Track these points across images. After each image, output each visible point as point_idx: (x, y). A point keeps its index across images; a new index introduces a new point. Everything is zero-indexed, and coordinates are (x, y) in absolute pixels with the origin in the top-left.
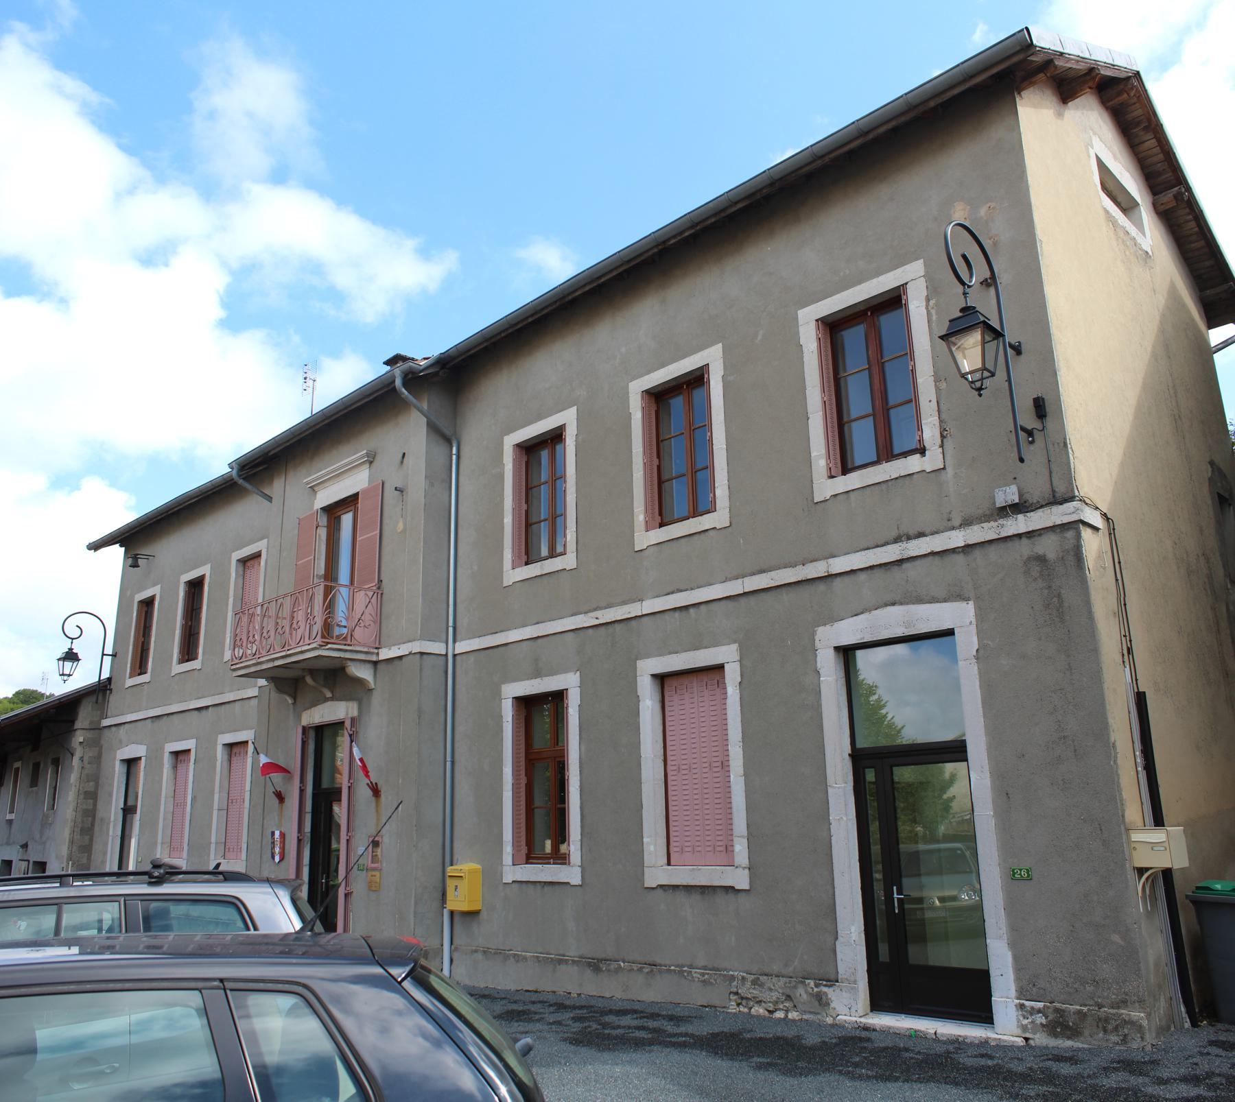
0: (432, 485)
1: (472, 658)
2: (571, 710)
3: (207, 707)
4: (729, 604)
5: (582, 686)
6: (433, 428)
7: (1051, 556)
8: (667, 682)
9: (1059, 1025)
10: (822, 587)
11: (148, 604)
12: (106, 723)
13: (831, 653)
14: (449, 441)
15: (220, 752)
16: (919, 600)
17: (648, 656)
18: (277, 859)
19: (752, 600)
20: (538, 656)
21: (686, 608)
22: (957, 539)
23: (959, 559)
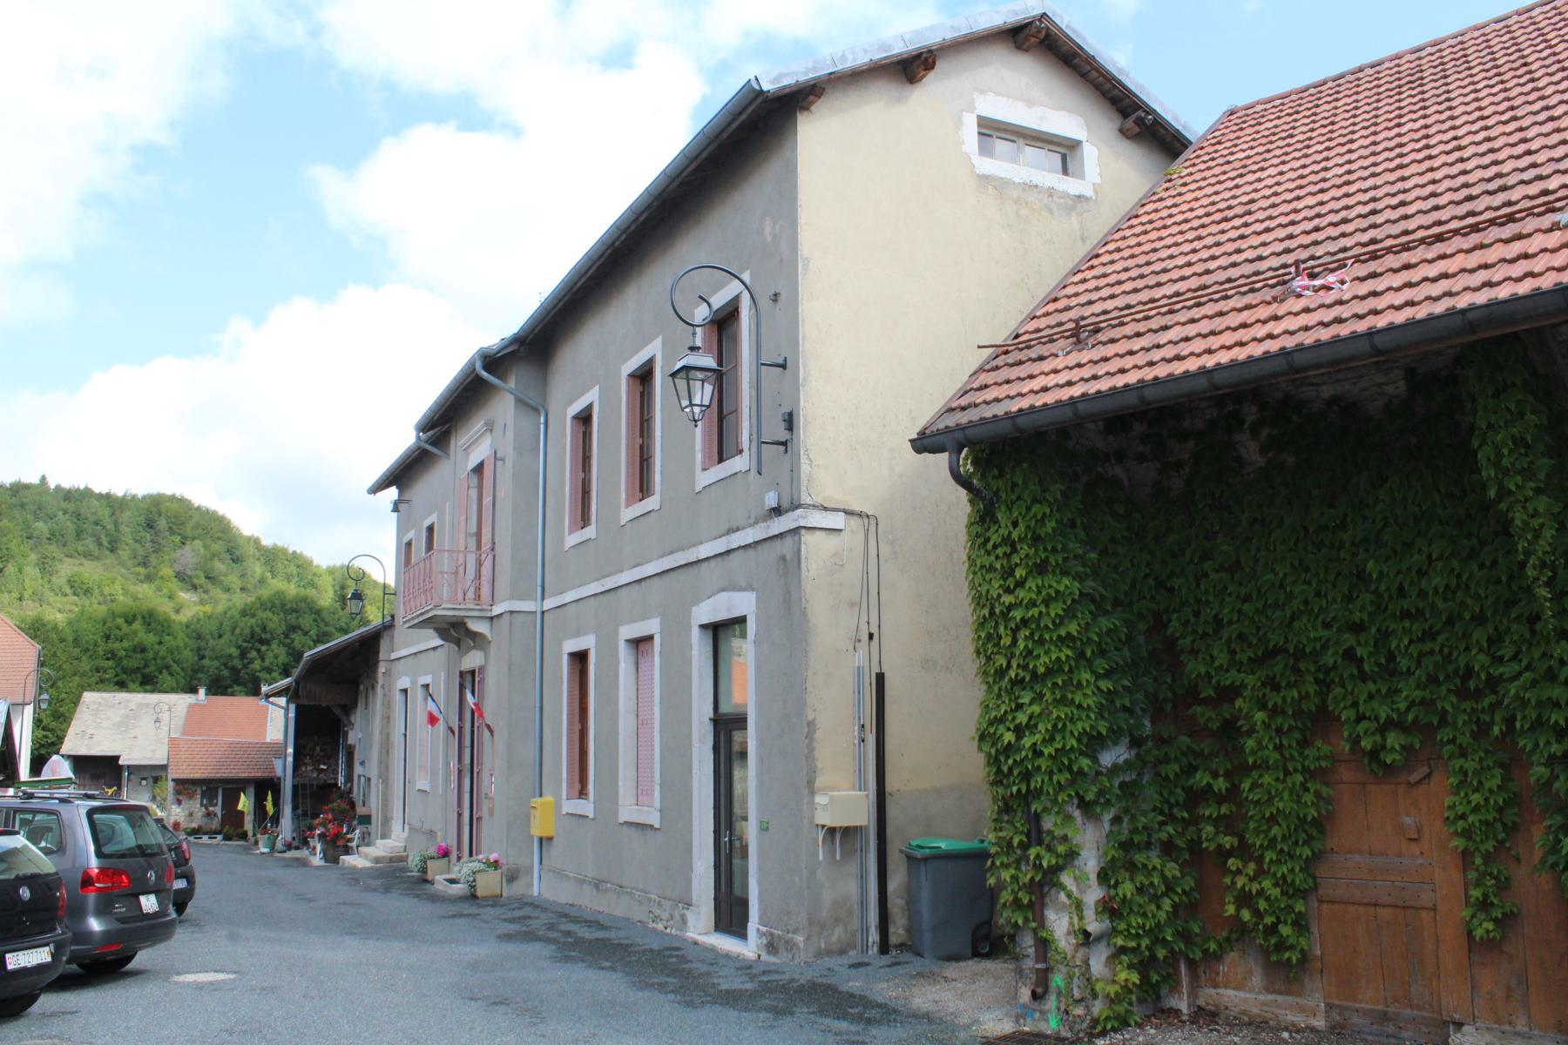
0: (521, 454)
6: (520, 401)
9: (771, 947)
11: (409, 544)
12: (393, 656)
14: (537, 411)
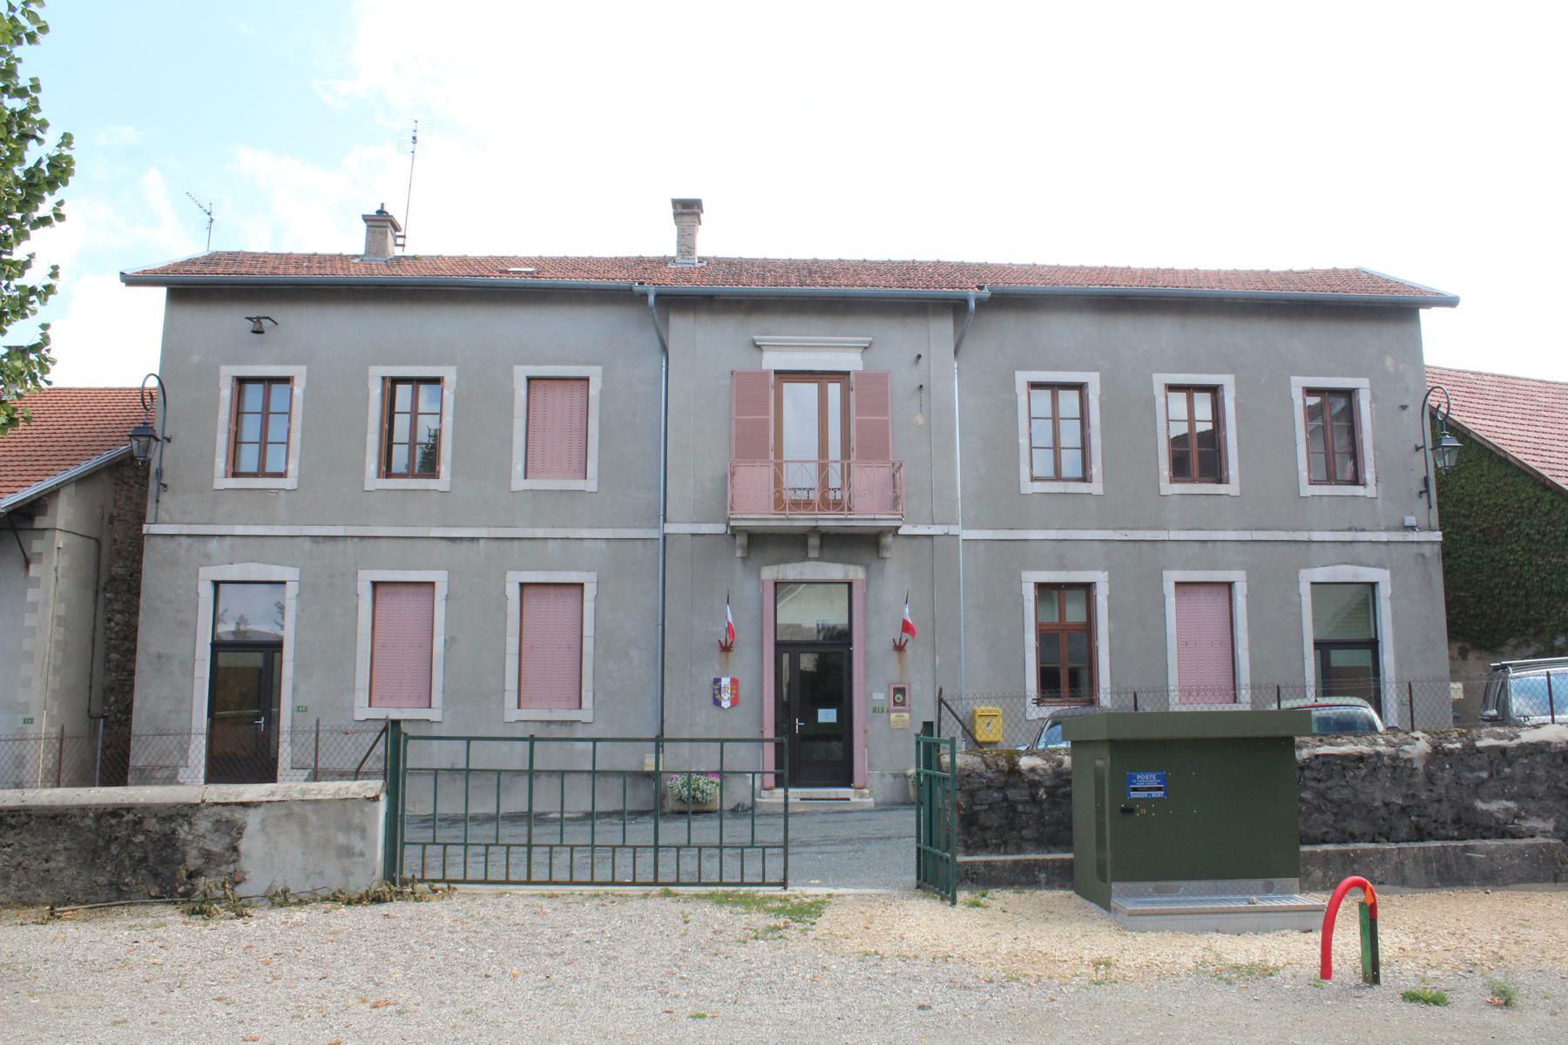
1: (982, 546)
2: (1099, 598)
3: (461, 539)
4: (1240, 546)
5: (1111, 581)
7: (1428, 554)
8: (380, 590)
10: (1303, 546)
13: (1032, 586)
15: (513, 592)
16: (1361, 564)
17: (1171, 568)
18: (725, 681)
19: (1256, 546)
20: (1061, 553)
22: (1383, 536)
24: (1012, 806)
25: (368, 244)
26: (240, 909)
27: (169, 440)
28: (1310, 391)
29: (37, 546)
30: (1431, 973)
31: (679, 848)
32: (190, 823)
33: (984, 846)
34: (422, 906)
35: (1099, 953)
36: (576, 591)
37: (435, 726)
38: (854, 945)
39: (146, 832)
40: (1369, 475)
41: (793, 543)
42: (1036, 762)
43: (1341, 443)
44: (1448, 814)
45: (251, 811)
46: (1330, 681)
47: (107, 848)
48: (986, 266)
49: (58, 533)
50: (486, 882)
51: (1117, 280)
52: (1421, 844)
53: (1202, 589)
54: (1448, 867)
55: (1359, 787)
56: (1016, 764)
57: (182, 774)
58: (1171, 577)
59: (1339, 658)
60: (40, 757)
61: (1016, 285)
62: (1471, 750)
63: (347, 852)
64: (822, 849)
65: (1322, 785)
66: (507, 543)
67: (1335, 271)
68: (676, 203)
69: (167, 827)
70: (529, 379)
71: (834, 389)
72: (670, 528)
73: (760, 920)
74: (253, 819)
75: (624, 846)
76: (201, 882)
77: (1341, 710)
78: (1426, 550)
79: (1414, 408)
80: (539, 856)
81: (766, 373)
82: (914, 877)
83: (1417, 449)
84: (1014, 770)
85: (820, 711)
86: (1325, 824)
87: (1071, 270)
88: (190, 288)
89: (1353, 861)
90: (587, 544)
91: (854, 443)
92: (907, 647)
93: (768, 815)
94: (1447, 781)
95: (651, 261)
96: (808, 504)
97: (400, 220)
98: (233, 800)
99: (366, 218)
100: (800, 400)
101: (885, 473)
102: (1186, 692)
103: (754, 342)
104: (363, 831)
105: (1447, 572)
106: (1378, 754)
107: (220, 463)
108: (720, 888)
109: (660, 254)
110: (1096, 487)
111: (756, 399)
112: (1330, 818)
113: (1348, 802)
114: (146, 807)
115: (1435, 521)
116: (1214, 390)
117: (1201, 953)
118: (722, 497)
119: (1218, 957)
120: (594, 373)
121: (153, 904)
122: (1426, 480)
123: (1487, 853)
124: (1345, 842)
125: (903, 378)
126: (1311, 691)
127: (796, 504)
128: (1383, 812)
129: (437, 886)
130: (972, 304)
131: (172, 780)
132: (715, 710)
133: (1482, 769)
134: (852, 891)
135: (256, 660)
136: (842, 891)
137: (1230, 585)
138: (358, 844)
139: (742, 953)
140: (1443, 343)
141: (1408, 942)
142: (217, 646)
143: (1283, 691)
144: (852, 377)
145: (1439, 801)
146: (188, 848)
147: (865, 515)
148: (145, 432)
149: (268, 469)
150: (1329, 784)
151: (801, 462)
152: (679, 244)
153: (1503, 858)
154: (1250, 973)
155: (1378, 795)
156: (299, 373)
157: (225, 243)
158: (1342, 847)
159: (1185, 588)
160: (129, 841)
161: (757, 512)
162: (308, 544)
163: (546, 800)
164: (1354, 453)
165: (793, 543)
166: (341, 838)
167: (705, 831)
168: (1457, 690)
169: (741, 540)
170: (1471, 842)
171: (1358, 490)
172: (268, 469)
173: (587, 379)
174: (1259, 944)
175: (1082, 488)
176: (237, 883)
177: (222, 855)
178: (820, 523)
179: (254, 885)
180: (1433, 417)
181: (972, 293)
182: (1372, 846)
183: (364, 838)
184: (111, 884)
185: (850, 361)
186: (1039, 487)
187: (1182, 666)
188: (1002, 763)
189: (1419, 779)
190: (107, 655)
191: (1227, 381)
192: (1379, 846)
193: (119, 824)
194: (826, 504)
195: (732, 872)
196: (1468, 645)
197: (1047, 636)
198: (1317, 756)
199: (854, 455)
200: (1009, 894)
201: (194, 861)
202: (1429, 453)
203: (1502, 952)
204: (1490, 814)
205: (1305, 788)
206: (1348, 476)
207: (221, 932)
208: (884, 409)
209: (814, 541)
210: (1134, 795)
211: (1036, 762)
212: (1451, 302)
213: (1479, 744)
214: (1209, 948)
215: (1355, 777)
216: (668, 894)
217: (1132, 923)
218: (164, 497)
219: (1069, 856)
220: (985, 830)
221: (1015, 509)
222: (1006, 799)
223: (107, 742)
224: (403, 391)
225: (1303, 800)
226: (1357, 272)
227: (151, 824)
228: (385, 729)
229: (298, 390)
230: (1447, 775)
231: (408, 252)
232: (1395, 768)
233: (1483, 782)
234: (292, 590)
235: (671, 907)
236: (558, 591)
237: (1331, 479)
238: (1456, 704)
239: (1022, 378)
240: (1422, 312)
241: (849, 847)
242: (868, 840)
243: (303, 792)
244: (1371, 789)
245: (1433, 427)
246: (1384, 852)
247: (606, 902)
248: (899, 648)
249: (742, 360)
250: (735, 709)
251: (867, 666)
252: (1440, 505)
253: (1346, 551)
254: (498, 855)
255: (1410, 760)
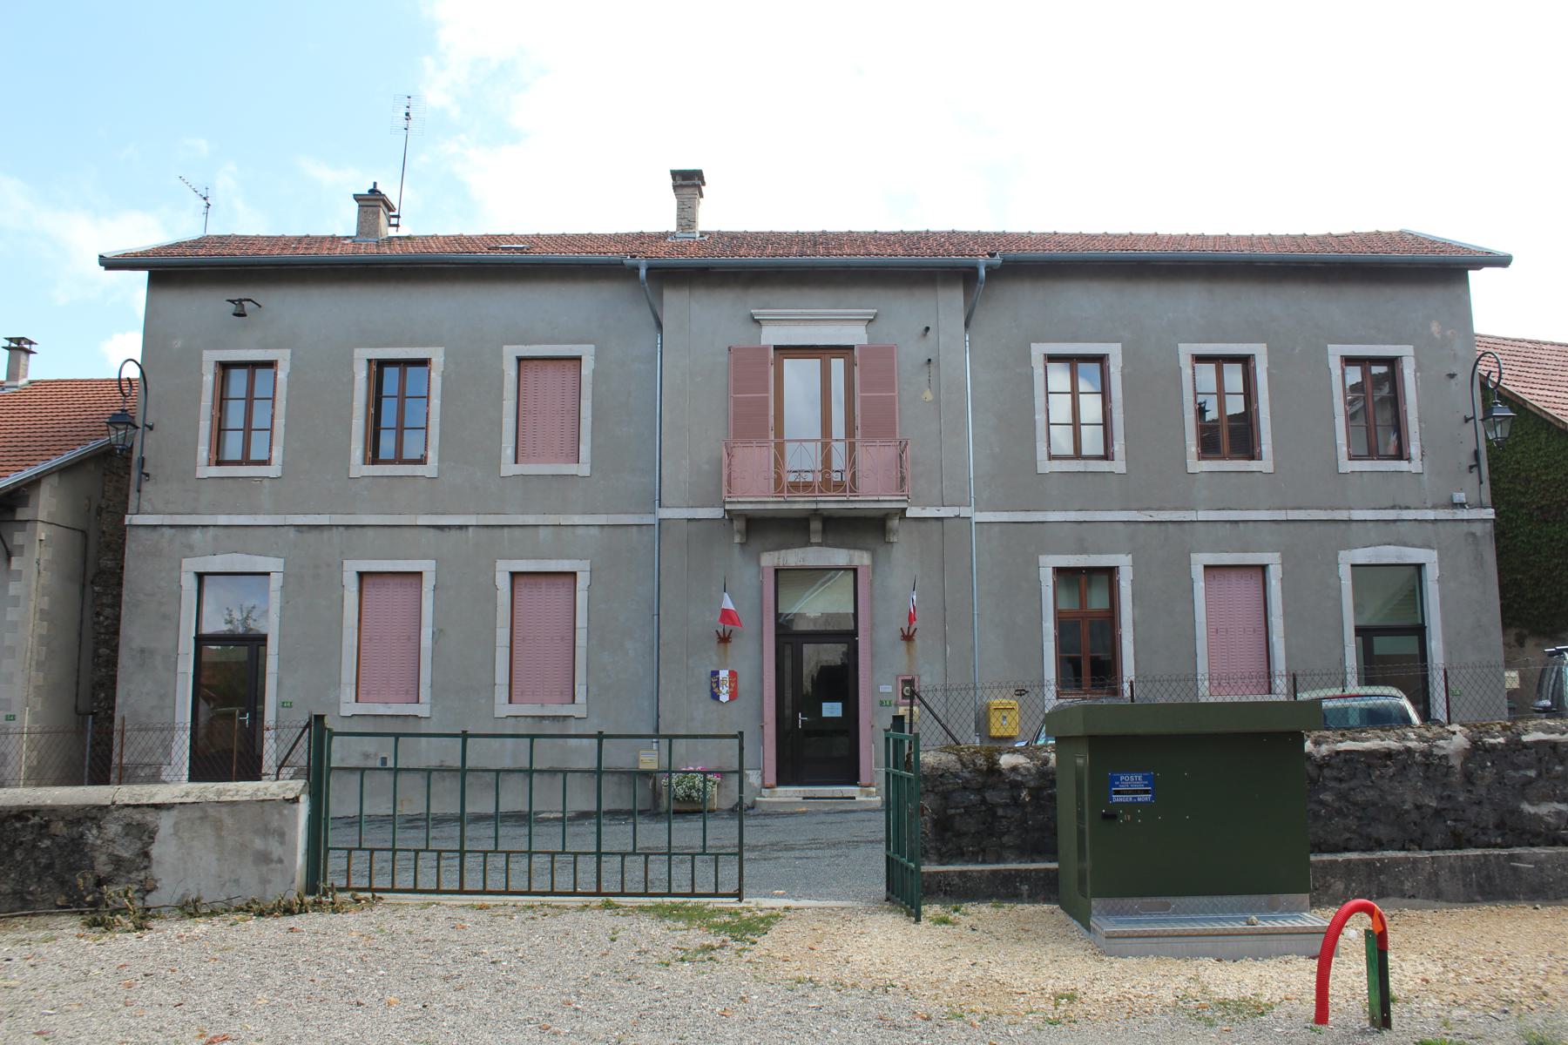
1: (997, 528)
2: (1122, 583)
3: (449, 527)
4: (1274, 526)
5: (1135, 565)
7: (1478, 534)
10: (1343, 526)
13: (1050, 571)
15: (503, 582)
16: (1405, 545)
18: (724, 674)
19: (1291, 526)
20: (1081, 535)
21: (1237, 522)
22: (1430, 515)
23: (1429, 526)
24: (992, 809)
25: (360, 224)
26: (142, 923)
27: (151, 428)
28: (1349, 361)
29: (18, 538)
30: (1457, 1013)
31: (623, 855)
32: (99, 827)
33: (959, 855)
34: (336, 919)
35: (1064, 984)
36: (569, 580)
37: (423, 722)
38: (791, 970)
39: (53, 837)
40: (1414, 449)
41: (793, 527)
42: (1019, 760)
43: (1384, 417)
44: (1491, 819)
45: (164, 814)
46: (1374, 670)
47: (11, 853)
48: (1004, 235)
49: (40, 525)
50: (414, 891)
51: (1141, 245)
52: (1459, 853)
53: (1233, 574)
54: (1489, 878)
55: (1386, 788)
56: (996, 762)
57: (166, 773)
58: (1200, 560)
59: (1382, 645)
60: (21, 754)
61: (1029, 252)
62: (1516, 745)
63: (264, 858)
64: (803, 854)
65: (1344, 786)
66: (496, 531)
67: (1378, 233)
68: (674, 174)
69: (75, 832)
70: (520, 360)
71: (838, 365)
72: (665, 513)
73: (697, 937)
74: (165, 822)
75: (496, 851)
76: (109, 890)
77: (1380, 701)
78: (1477, 529)
79: (1463, 376)
80: (472, 862)
81: (766, 348)
82: (884, 888)
83: (1467, 420)
84: (993, 769)
85: (825, 705)
86: (1347, 829)
87: (1094, 237)
88: (170, 272)
89: (1380, 871)
90: (579, 531)
91: (858, 422)
92: (916, 637)
93: (767, 815)
94: (1488, 781)
95: (650, 236)
96: (807, 486)
97: (394, 201)
98: (145, 801)
99: (357, 198)
100: (800, 377)
101: (891, 452)
102: (1216, 681)
103: (752, 316)
104: (282, 835)
105: (1501, 555)
106: (1408, 750)
107: (203, 451)
108: (667, 900)
109: (663, 229)
110: (1118, 465)
111: (755, 374)
112: (1352, 823)
113: (1374, 804)
114: (53, 810)
115: (1486, 497)
116: (1245, 361)
117: (1185, 985)
118: (719, 479)
119: (1204, 991)
120: (587, 352)
121: (58, 915)
122: (1476, 454)
123: (1536, 863)
124: (1371, 849)
125: (910, 352)
126: (1352, 678)
127: (795, 486)
128: (1415, 816)
129: (361, 895)
130: (983, 272)
131: (155, 779)
132: (713, 703)
133: (1529, 767)
134: (813, 903)
135: (241, 653)
136: (804, 903)
137: (1263, 568)
138: (276, 850)
139: (659, 978)
140: (1496, 309)
141: (1433, 971)
142: (201, 640)
143: (1299, 679)
144: (856, 352)
145: (1479, 803)
146: (97, 854)
147: (871, 496)
148: (122, 419)
149: (252, 457)
150: (1353, 784)
151: (801, 441)
152: (680, 218)
153: (1554, 869)
154: (1238, 1011)
155: (1409, 797)
156: (282, 356)
157: (218, 227)
158: (1366, 856)
159: (1215, 572)
160: (34, 846)
161: (756, 495)
162: (292, 533)
163: (547, 801)
164: (1398, 426)
165: (793, 527)
166: (258, 843)
167: (687, 833)
168: (1512, 679)
169: (739, 525)
170: (1517, 850)
171: (1403, 465)
172: (252, 457)
173: (579, 359)
174: (1255, 972)
175: (1104, 466)
176: (149, 892)
177: (132, 861)
178: (821, 506)
179: (163, 896)
180: (1484, 386)
181: (982, 261)
182: (1401, 854)
183: (282, 843)
184: (15, 893)
185: (854, 335)
186: (1057, 466)
187: (1203, 651)
188: (981, 761)
189: (1456, 778)
190: (95, 651)
191: (1259, 351)
192: (1410, 855)
193: (24, 827)
194: (827, 485)
195: (681, 882)
196: (1526, 632)
197: (1064, 624)
198: (1338, 753)
199: (858, 434)
200: (986, 909)
201: (103, 867)
202: (1479, 424)
203: (1547, 986)
204: (1537, 818)
205: (1325, 789)
206: (1392, 450)
207: (124, 945)
208: (890, 385)
209: (816, 525)
210: (1117, 798)
211: (1019, 760)
212: (1503, 261)
213: (1525, 738)
214: (1196, 979)
215: (1381, 777)
216: (608, 906)
217: (1111, 947)
218: (146, 487)
219: (1054, 865)
220: (972, 839)
221: (1037, 490)
222: (983, 801)
223: (91, 735)
224: (391, 374)
225: (1322, 803)
226: (1401, 234)
227: (59, 828)
228: (308, 725)
229: (282, 375)
230: (1489, 774)
231: (403, 232)
232: (1428, 766)
233: (1530, 781)
234: (276, 581)
235: (607, 920)
236: (551, 580)
237: (1373, 453)
238: (1511, 694)
239: (1039, 350)
240: (1471, 273)
241: (834, 852)
242: (856, 844)
243: (219, 793)
244: (1401, 790)
245: (1485, 399)
246: (1415, 861)
247: (538, 915)
248: (908, 638)
249: (741, 336)
250: (735, 704)
251: (873, 656)
252: (1493, 483)
253: (1389, 531)
254: (427, 861)
255: (1446, 757)
